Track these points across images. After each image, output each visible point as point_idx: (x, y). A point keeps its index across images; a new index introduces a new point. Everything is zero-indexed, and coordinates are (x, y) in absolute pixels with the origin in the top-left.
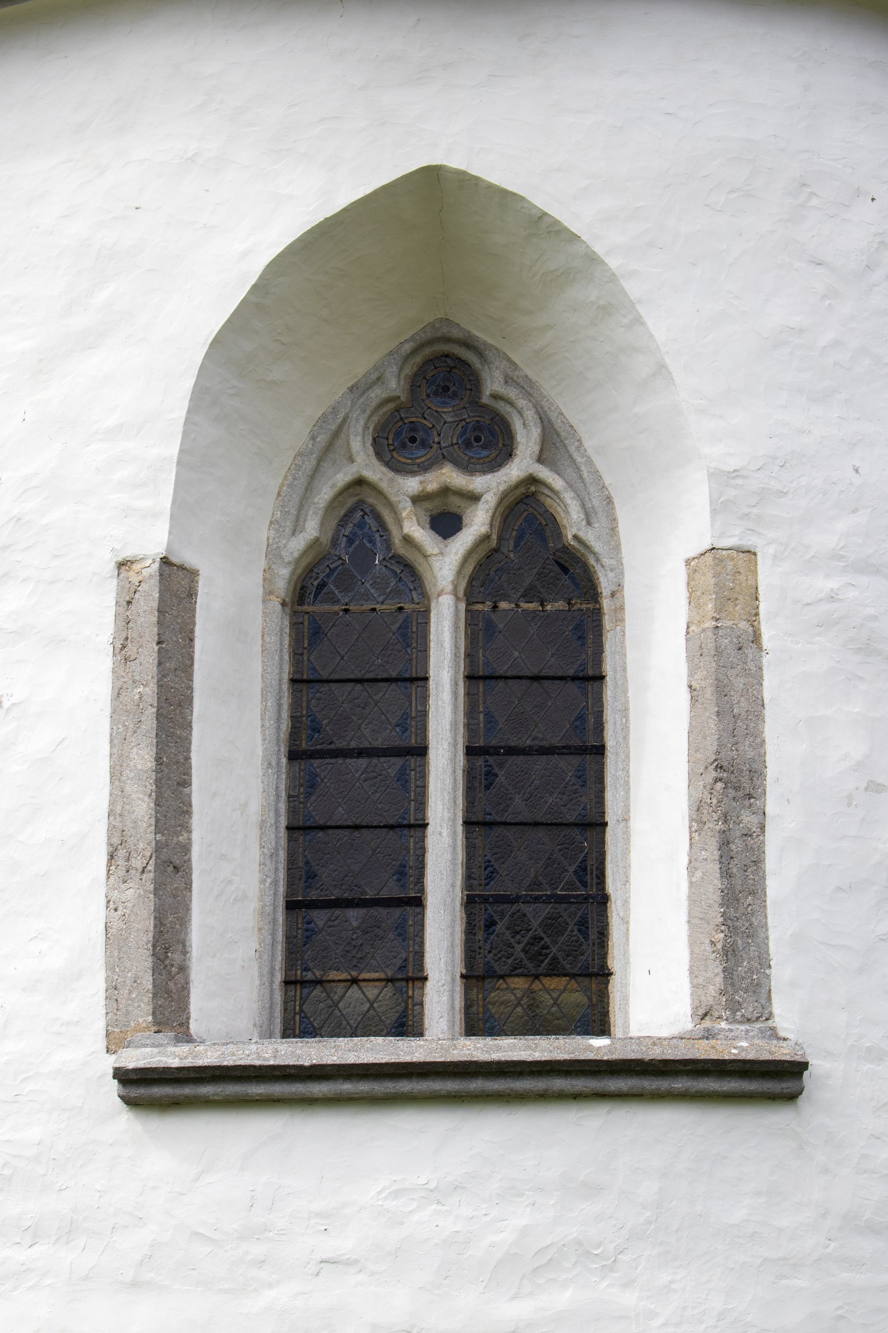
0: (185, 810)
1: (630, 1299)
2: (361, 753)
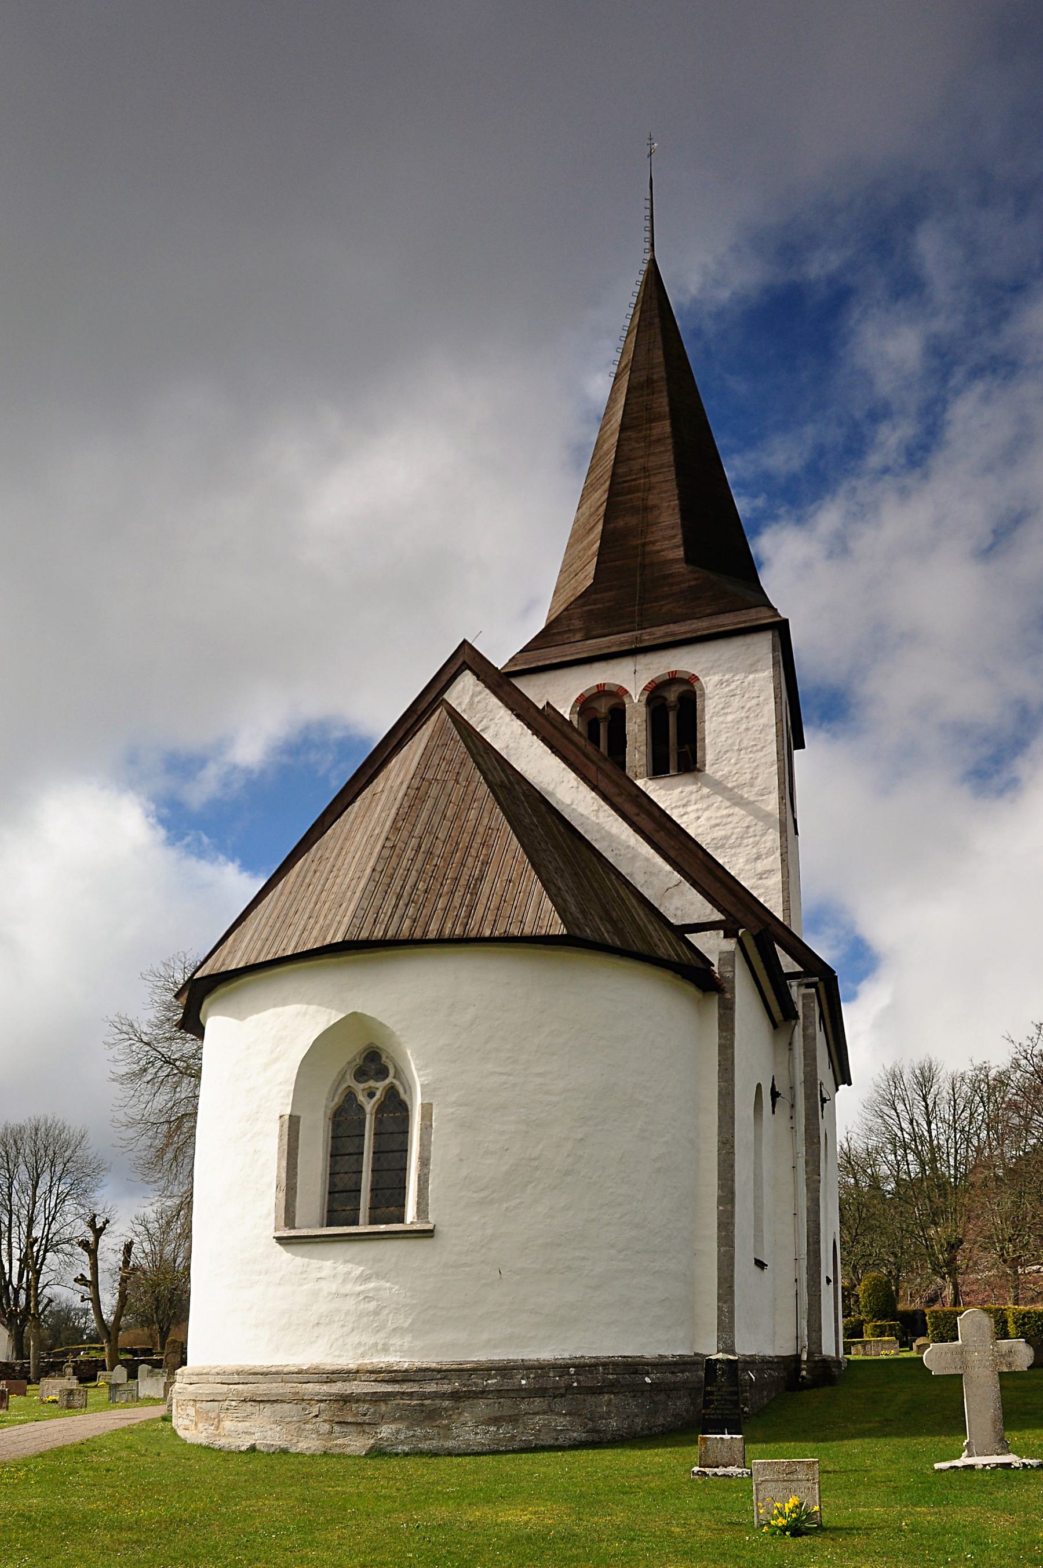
0: (296, 1174)
1: (388, 1284)
2: (348, 1155)
